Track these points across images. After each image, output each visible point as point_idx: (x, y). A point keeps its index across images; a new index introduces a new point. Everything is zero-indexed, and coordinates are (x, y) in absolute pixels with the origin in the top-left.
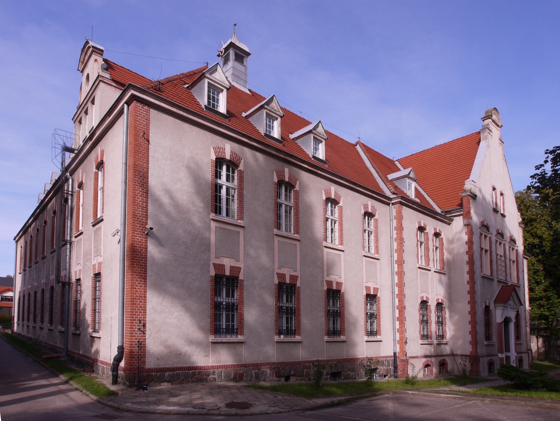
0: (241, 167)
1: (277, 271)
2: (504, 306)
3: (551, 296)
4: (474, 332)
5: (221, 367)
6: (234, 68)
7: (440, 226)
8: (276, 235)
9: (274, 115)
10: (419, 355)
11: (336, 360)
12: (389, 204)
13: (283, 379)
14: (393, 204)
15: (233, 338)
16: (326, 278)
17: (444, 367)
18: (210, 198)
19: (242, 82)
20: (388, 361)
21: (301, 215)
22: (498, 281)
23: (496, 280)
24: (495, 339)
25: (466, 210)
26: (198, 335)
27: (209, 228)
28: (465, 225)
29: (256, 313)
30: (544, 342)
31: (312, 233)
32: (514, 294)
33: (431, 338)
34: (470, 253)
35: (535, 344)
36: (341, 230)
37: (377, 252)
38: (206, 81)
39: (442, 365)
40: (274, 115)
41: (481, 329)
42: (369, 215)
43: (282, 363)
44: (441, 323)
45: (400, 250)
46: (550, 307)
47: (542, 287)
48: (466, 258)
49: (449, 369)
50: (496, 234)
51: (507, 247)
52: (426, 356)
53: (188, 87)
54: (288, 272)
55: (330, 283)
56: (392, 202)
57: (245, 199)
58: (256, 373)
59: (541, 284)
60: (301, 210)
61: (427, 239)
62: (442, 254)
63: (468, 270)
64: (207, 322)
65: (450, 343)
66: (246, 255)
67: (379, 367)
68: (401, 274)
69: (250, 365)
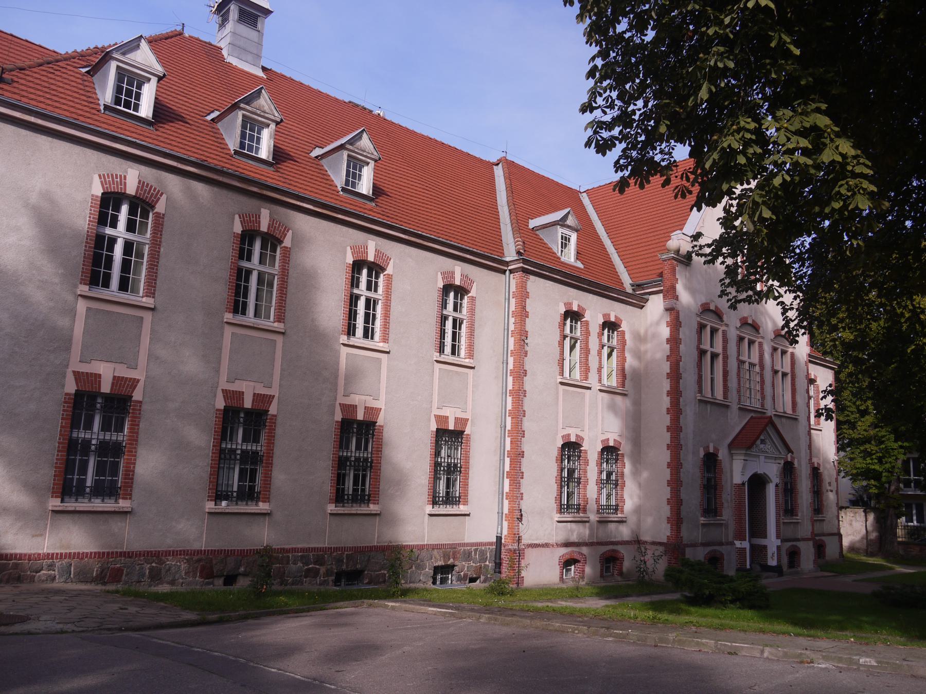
0: (160, 207)
1: (224, 385)
2: (746, 455)
3: (884, 436)
4: (676, 502)
5: (69, 555)
6: (234, 33)
7: (616, 310)
8: (227, 323)
9: (260, 119)
10: (553, 540)
11: (351, 549)
12: (504, 272)
13: (220, 581)
14: (511, 271)
15: (109, 505)
16: (341, 400)
17: (611, 567)
18: (80, 260)
19: (250, 58)
20: (483, 553)
21: (291, 289)
22: (740, 409)
23: (735, 407)
24: (727, 514)
25: (668, 284)
26: (19, 498)
27: (72, 313)
28: (667, 310)
29: (165, 460)
30: (878, 520)
31: (313, 320)
32: (770, 430)
33: (585, 511)
34: (674, 358)
35: (854, 527)
36: (386, 316)
37: (471, 355)
38: (113, 65)
39: (610, 561)
40: (260, 119)
41: (693, 497)
42: (455, 290)
43: (220, 552)
44: (611, 481)
45: (521, 351)
46: (884, 457)
47: (869, 419)
48: (666, 367)
49: (624, 569)
50: (739, 325)
51: (767, 349)
52: (567, 544)
53: (88, 72)
54: (249, 390)
55: (349, 409)
56: (510, 268)
57: (162, 261)
58: (151, 569)
59: (869, 414)
60: (292, 280)
61: (587, 333)
62: (622, 360)
63: (668, 389)
64: (47, 474)
65: (632, 520)
66: (151, 356)
67: (457, 563)
68: (519, 394)
69: (139, 554)
